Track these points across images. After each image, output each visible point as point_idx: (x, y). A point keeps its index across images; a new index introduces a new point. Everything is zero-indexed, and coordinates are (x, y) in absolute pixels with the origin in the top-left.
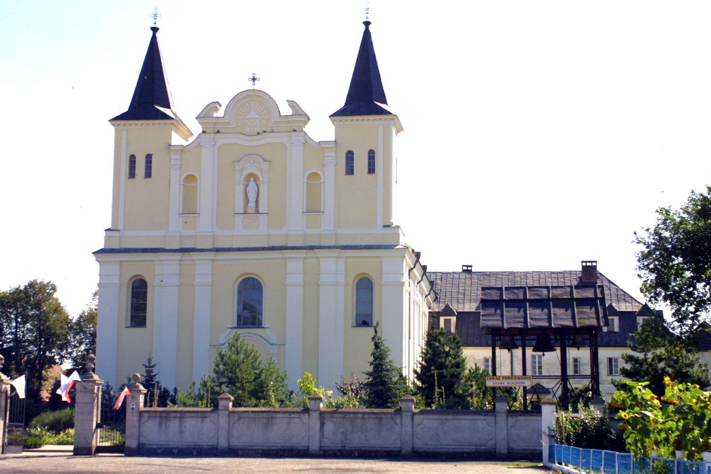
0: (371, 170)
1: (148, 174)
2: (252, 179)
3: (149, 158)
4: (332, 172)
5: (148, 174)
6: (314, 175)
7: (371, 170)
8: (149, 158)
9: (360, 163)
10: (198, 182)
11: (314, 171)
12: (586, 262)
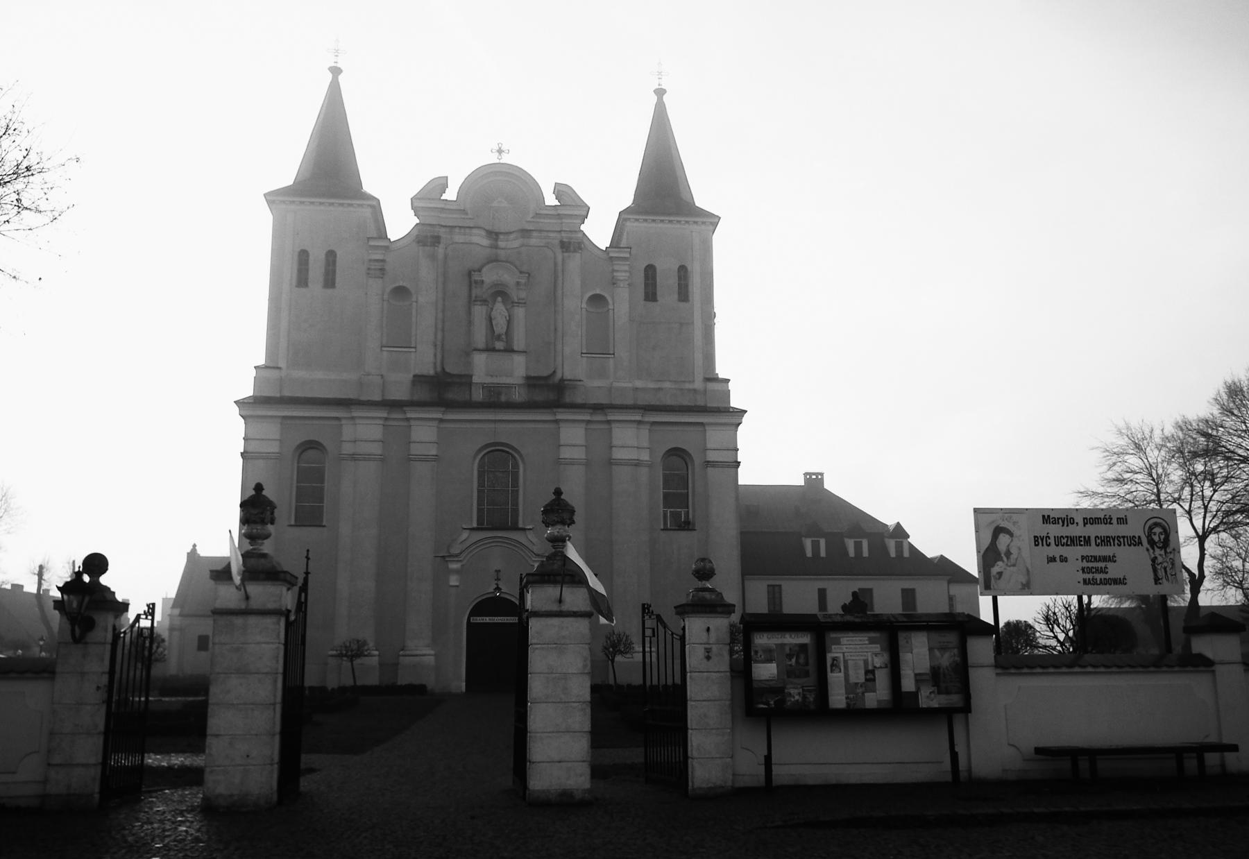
0: (303, 257)
2: (499, 299)
11: (598, 292)
12: (811, 474)
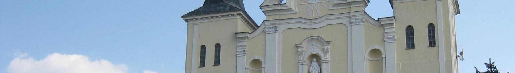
0: (432, 43)
1: (217, 62)
3: (218, 47)
4: (394, 50)
5: (217, 62)
6: (375, 52)
7: (432, 43)
8: (218, 47)
9: (421, 36)
10: (383, 56)
